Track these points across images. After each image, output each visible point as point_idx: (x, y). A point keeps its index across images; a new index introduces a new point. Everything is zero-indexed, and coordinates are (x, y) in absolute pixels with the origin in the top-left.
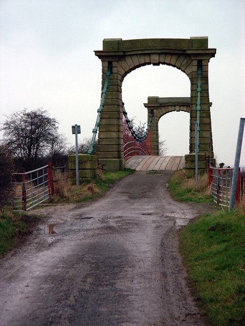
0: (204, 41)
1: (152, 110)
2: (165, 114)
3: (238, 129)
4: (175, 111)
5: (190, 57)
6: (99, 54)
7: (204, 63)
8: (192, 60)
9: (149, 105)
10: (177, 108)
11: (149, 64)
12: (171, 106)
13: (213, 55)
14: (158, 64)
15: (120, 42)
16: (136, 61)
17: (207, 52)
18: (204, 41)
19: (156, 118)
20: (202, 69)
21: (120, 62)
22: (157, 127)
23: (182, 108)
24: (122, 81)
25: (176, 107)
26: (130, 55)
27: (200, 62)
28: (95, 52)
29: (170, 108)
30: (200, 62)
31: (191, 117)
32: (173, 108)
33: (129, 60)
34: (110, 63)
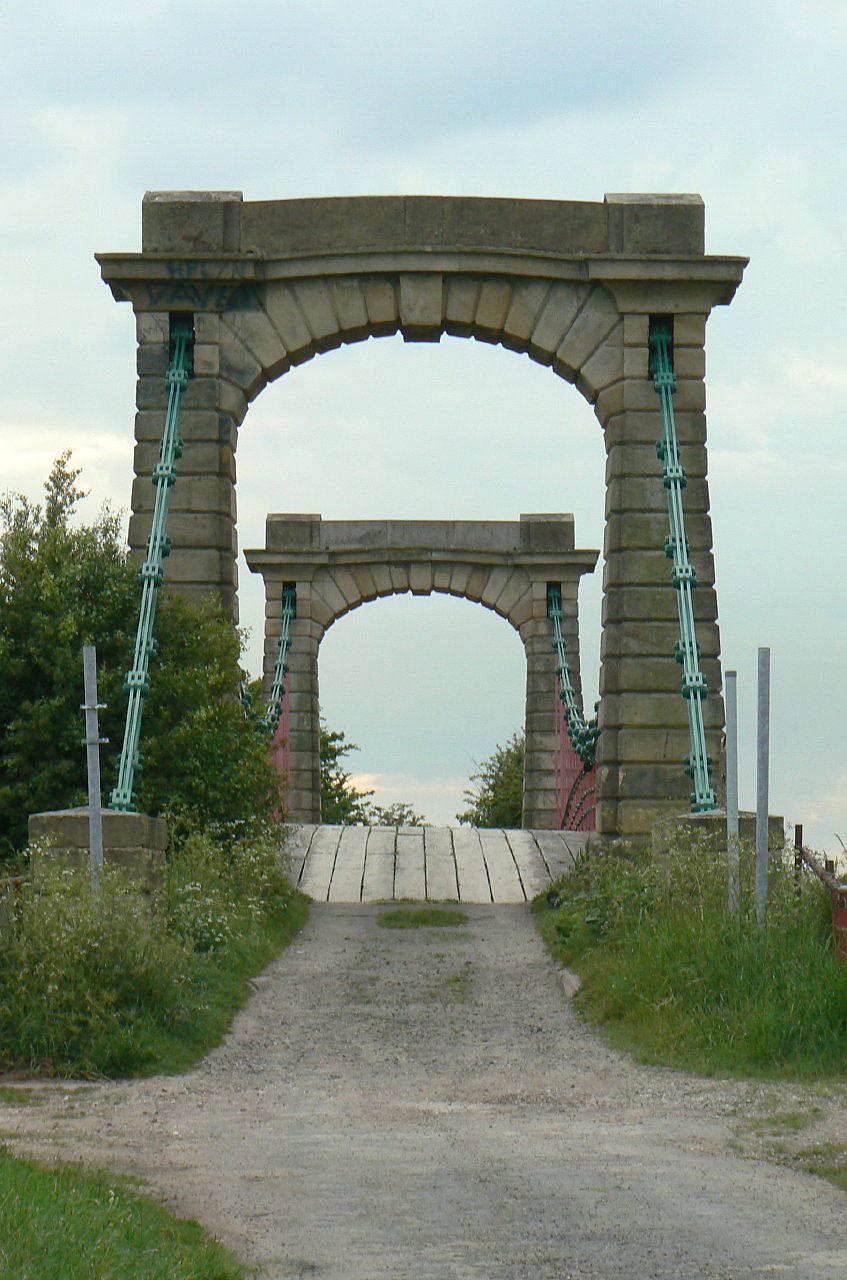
0: (684, 217)
1: (290, 586)
2: (384, 594)
3: (757, 724)
4: (404, 591)
5: (611, 297)
6: (126, 272)
8: (622, 316)
9: (277, 559)
10: (420, 577)
11: (383, 330)
12: (389, 563)
13: (724, 291)
14: (428, 334)
15: (228, 210)
16: (319, 310)
17: (702, 273)
18: (684, 217)
19: (306, 626)
20: (671, 362)
21: (229, 317)
22: (312, 672)
23: (442, 580)
24: (250, 395)
25: (414, 570)
26: (289, 283)
27: (661, 322)
28: (101, 259)
29: (383, 579)
30: (661, 322)
31: (314, 711)
32: (398, 576)
33: (279, 303)
34: (181, 321)
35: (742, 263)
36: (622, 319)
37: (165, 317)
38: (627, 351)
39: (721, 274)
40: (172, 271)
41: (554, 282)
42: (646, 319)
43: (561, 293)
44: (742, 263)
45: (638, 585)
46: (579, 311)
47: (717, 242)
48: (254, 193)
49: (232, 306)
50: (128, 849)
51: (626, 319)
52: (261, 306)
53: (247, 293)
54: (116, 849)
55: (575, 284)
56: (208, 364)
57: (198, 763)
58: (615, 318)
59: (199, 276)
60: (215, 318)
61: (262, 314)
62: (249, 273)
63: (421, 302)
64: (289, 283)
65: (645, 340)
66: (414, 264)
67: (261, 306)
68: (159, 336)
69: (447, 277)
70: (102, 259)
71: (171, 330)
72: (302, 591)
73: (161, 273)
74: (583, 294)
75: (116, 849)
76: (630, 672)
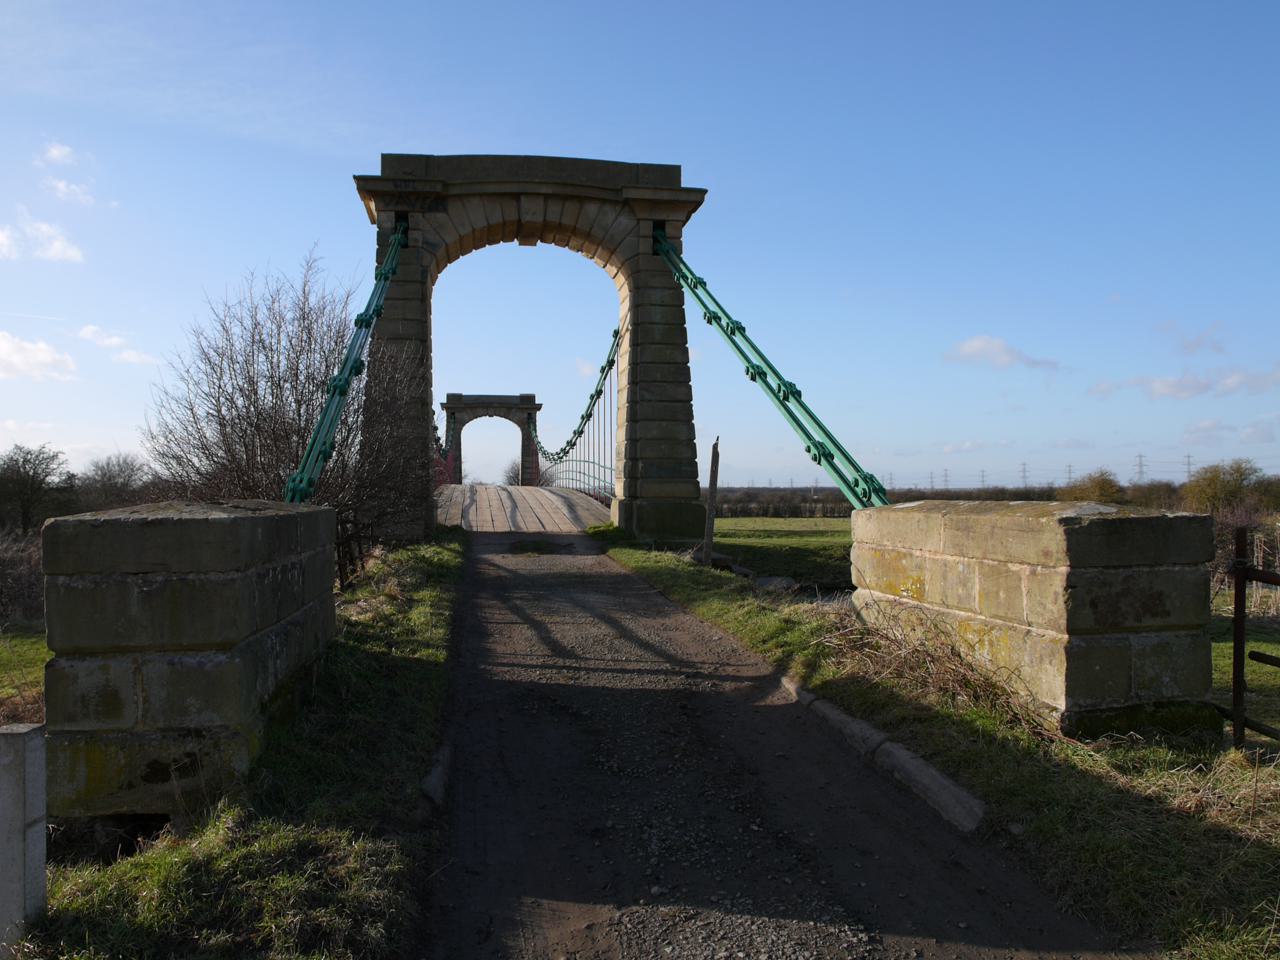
0: (674, 171)
1: (453, 414)
7: (669, 230)
8: (639, 220)
13: (539, 409)
18: (674, 171)
21: (427, 215)
26: (460, 196)
27: (659, 225)
30: (529, 414)
34: (401, 217)
35: (705, 191)
36: (638, 223)
37: (393, 214)
38: (641, 240)
39: (693, 197)
40: (396, 186)
41: (604, 201)
42: (651, 224)
43: (607, 208)
44: (705, 191)
45: (648, 363)
46: (616, 218)
47: (687, 182)
48: (464, 394)
49: (431, 209)
50: (213, 576)
51: (641, 222)
52: (445, 210)
53: (438, 202)
54: (191, 576)
55: (616, 203)
56: (416, 240)
57: (245, 457)
58: (636, 222)
59: (410, 189)
60: (420, 215)
61: (445, 215)
62: (439, 188)
63: (532, 211)
64: (460, 196)
65: (651, 233)
66: (531, 188)
67: (445, 210)
68: (389, 225)
69: (547, 197)
70: (358, 179)
71: (396, 222)
72: (457, 415)
73: (389, 187)
74: (618, 208)
75: (191, 576)
76: (526, 476)
